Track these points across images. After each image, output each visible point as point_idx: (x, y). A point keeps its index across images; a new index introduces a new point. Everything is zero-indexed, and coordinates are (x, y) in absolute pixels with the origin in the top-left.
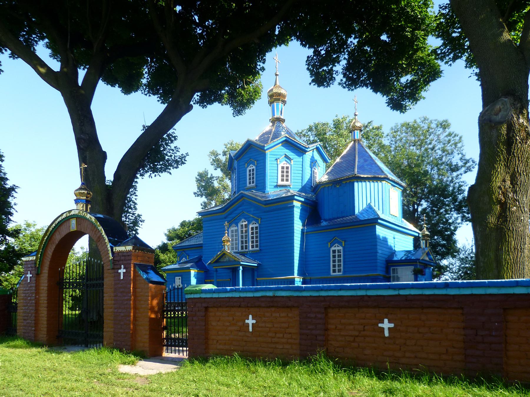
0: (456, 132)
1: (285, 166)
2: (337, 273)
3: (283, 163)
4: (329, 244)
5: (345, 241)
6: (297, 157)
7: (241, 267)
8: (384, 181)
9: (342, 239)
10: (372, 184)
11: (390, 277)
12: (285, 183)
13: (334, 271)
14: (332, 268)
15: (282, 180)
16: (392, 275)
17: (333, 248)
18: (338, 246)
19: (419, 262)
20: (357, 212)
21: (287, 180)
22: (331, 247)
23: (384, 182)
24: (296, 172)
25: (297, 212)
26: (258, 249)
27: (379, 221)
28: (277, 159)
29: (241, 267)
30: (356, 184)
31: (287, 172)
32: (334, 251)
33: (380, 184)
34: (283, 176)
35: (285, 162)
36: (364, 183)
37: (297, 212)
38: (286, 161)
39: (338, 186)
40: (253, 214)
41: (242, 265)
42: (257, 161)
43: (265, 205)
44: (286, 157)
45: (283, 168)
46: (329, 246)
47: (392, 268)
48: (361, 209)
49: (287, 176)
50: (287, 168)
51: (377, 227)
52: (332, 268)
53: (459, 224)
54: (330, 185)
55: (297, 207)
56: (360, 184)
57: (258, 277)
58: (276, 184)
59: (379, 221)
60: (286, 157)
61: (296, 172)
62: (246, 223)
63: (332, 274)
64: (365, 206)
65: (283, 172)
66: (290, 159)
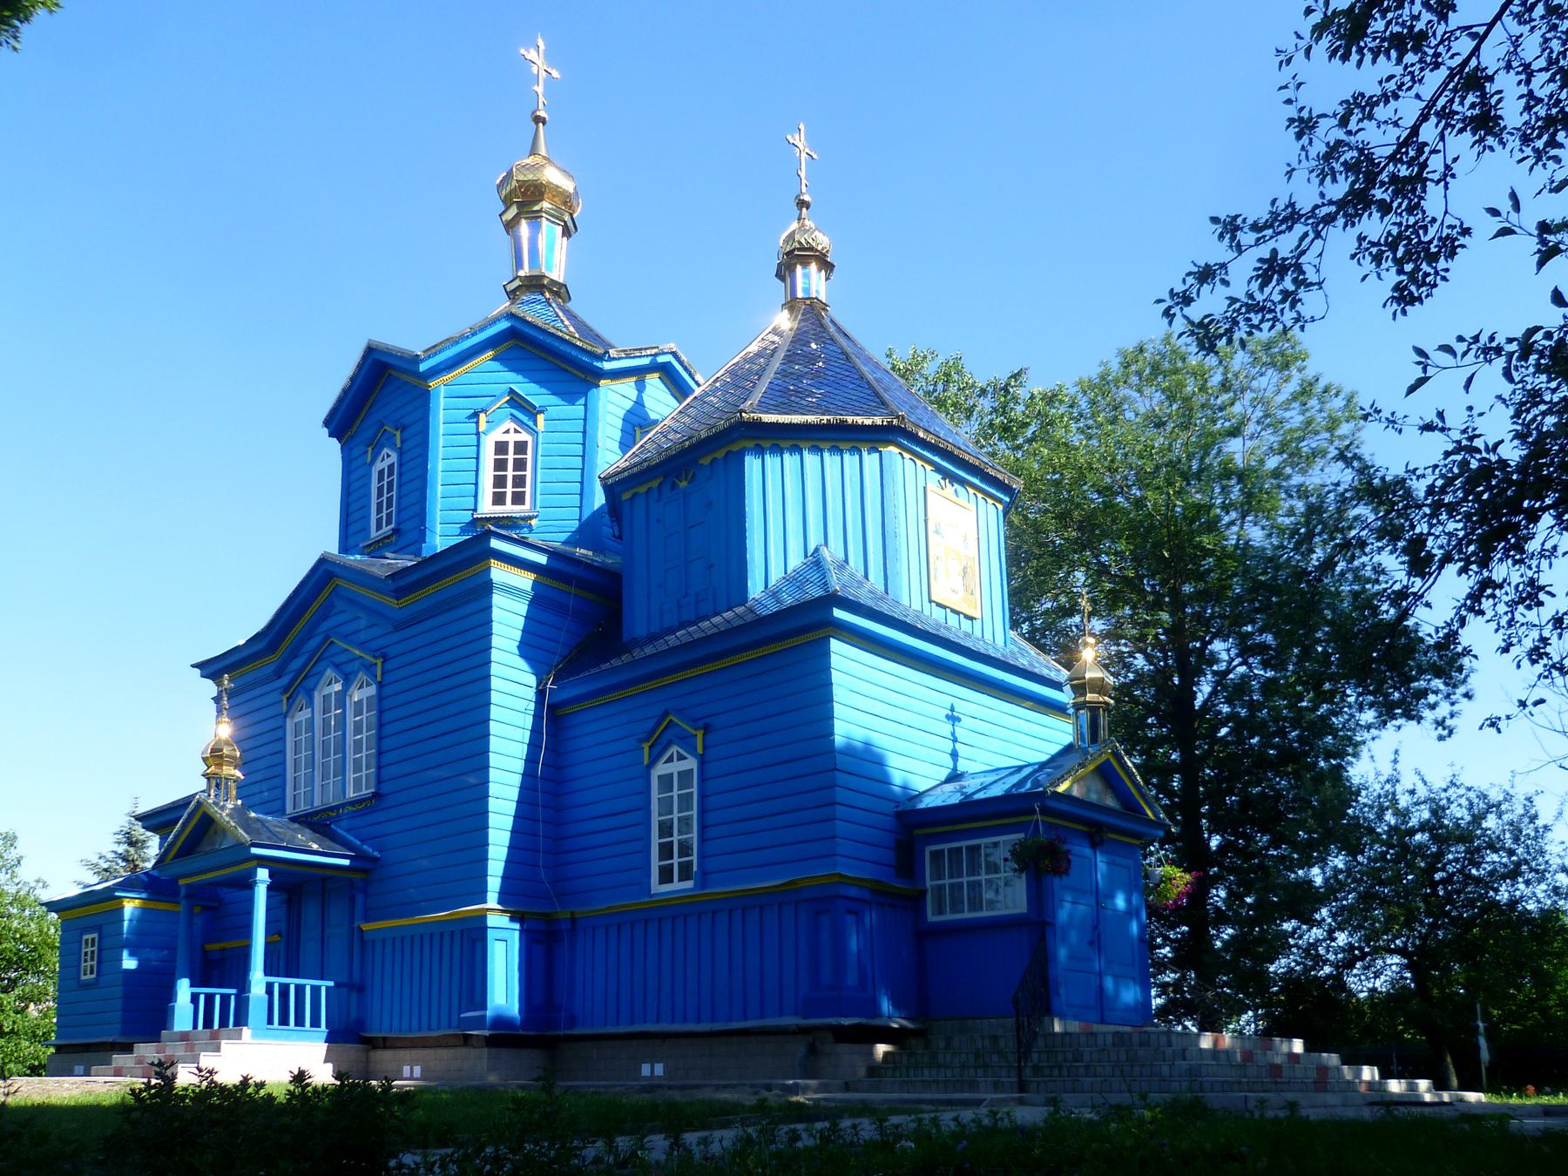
0: (1336, 382)
1: (512, 438)
2: (677, 885)
3: (502, 430)
4: (646, 746)
5: (707, 729)
6: (553, 399)
7: (263, 874)
8: (889, 442)
9: (694, 722)
10: (831, 460)
11: (924, 893)
12: (508, 509)
13: (666, 875)
14: (655, 863)
15: (499, 499)
16: (929, 883)
17: (661, 769)
18: (681, 758)
19: (1045, 811)
20: (755, 589)
21: (518, 499)
22: (654, 761)
23: (893, 449)
24: (559, 462)
25: (508, 616)
26: (689, 884)
27: (838, 613)
28: (476, 415)
29: (263, 874)
30: (752, 464)
31: (520, 465)
32: (666, 781)
33: (871, 460)
34: (499, 482)
35: (512, 426)
36: (790, 460)
37: (508, 616)
38: (514, 418)
39: (684, 484)
40: (361, 645)
41: (264, 861)
42: (404, 428)
43: (399, 593)
44: (516, 401)
45: (501, 447)
46: (646, 761)
47: (929, 849)
48: (776, 575)
49: (519, 481)
50: (521, 447)
51: (835, 645)
52: (655, 863)
53: (1368, 727)
54: (655, 484)
55: (510, 590)
56: (771, 461)
57: (367, 919)
58: (467, 517)
59: (838, 613)
60: (516, 401)
61: (559, 462)
62: (338, 687)
63: (657, 887)
64: (796, 560)
65: (500, 465)
66: (532, 411)
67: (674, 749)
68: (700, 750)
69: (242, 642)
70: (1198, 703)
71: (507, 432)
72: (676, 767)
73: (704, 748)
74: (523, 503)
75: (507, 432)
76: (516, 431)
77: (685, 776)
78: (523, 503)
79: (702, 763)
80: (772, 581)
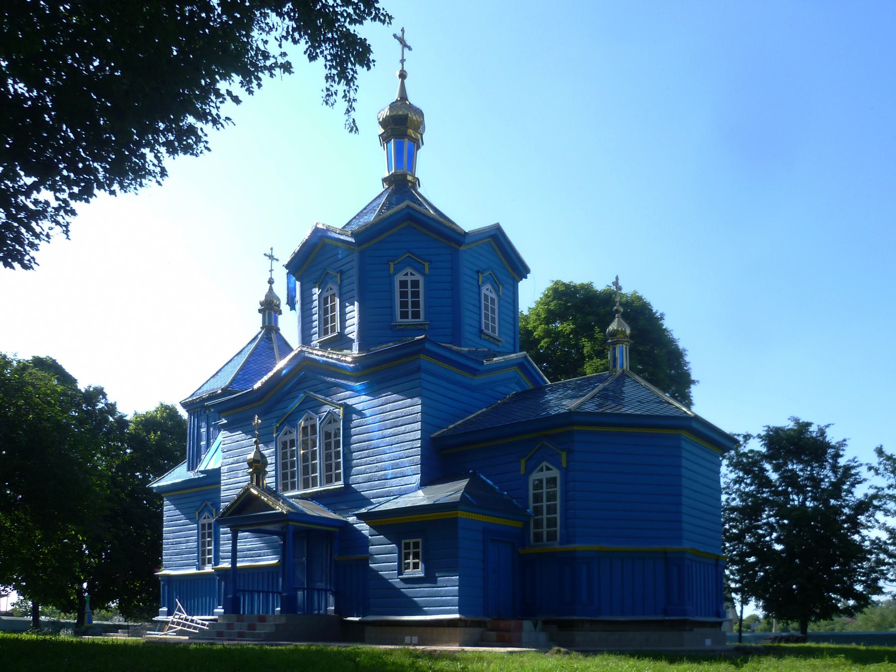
1: (409, 278)
4: (523, 462)
18: (548, 469)
22: (529, 471)
32: (539, 485)
45: (403, 284)
46: (523, 471)
65: (403, 295)
67: (544, 464)
68: (564, 465)
69: (282, 332)
70: (156, 619)
71: (407, 274)
72: (545, 475)
73: (568, 462)
74: (401, 282)
75: (407, 274)
76: (412, 274)
77: (552, 481)
78: (401, 282)
79: (565, 472)
80: (683, 470)
